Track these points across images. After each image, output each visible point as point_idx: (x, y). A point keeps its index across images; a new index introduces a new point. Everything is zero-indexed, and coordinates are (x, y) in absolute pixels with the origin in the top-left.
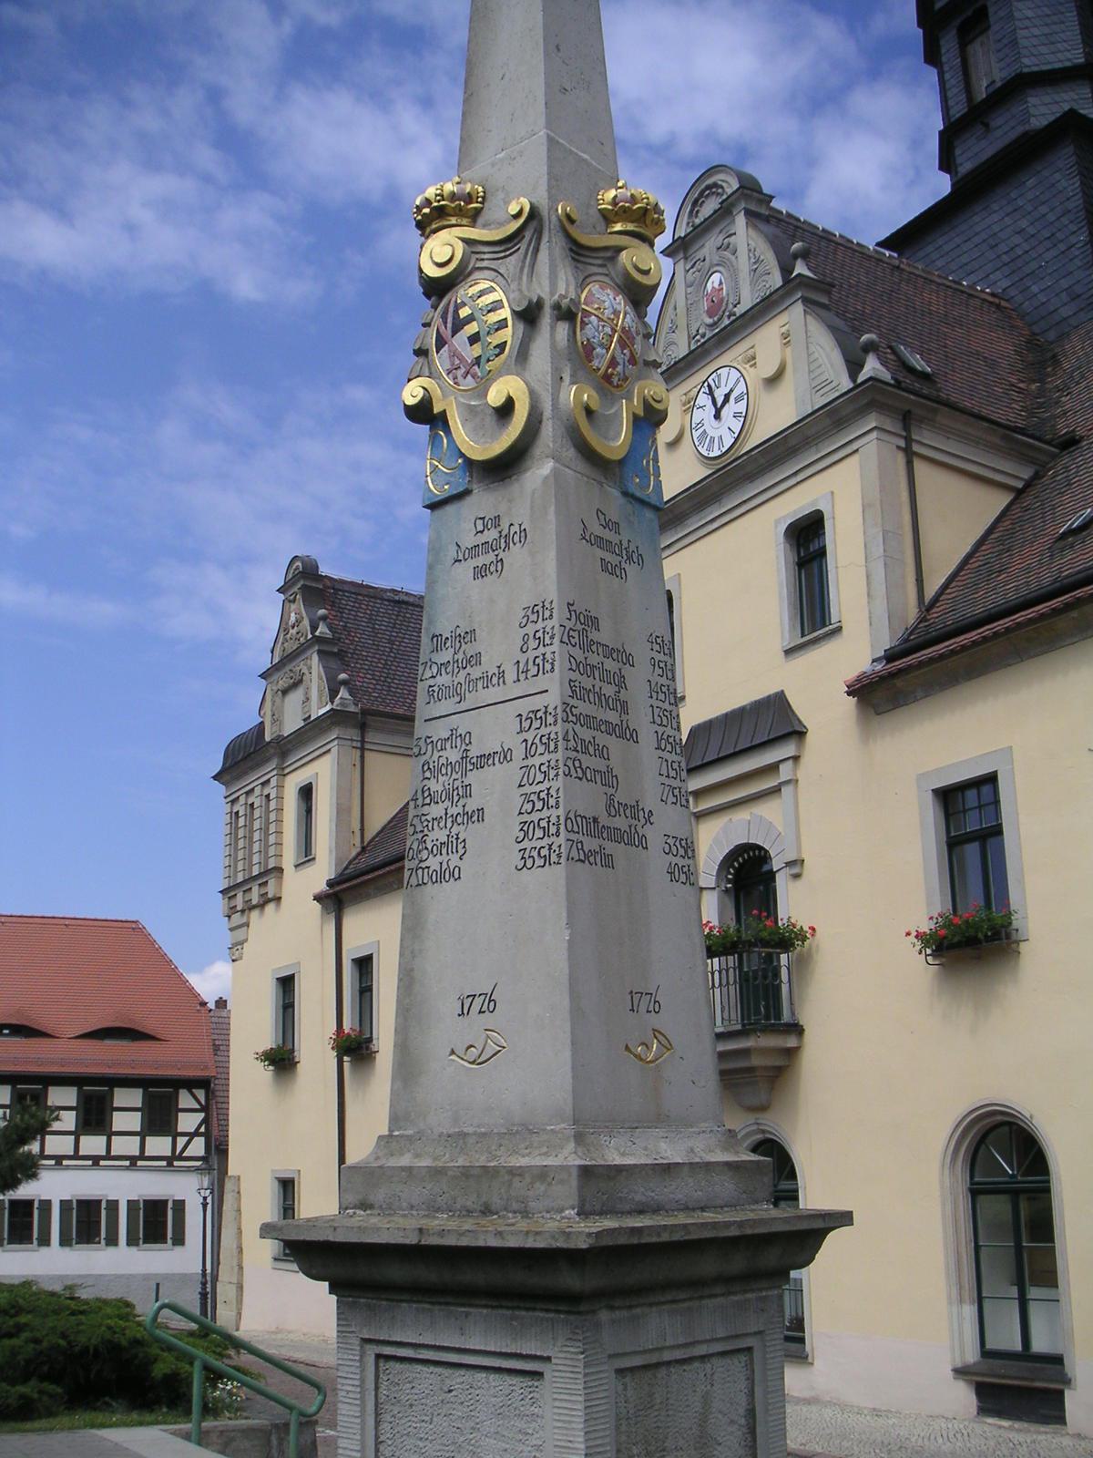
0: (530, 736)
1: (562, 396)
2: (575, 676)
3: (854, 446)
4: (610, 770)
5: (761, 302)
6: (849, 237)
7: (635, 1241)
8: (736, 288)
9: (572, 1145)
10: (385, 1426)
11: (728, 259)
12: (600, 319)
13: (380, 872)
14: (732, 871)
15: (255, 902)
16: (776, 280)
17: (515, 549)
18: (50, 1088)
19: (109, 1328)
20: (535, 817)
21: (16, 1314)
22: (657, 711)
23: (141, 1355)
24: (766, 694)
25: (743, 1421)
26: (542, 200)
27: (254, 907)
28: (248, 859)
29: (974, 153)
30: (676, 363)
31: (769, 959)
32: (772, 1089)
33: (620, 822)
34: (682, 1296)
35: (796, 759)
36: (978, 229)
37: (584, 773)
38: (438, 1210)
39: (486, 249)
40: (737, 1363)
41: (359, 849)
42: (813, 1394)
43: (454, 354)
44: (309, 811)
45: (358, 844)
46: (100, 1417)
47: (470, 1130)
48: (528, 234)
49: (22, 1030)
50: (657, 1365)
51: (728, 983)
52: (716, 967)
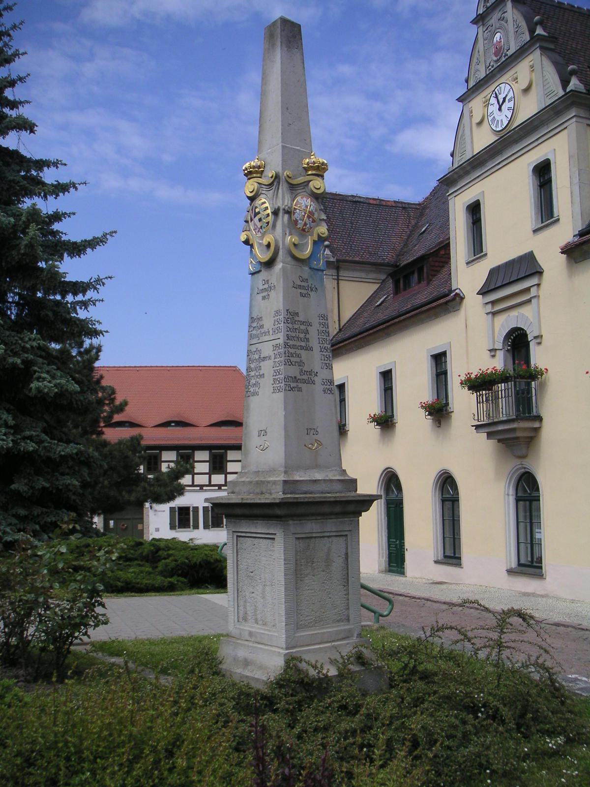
0: (275, 352)
1: (286, 241)
2: (289, 333)
3: (565, 125)
4: (301, 361)
5: (520, 48)
6: (573, 4)
7: (295, 501)
8: (508, 41)
9: (283, 474)
10: (239, 556)
11: (504, 26)
12: (300, 210)
13: (347, 342)
14: (510, 340)
16: (527, 37)
17: (272, 291)
18: (196, 452)
19: (206, 555)
20: (277, 377)
21: (168, 550)
22: (321, 339)
23: (219, 566)
24: (525, 253)
25: (344, 556)
26: (279, 169)
30: (480, 81)
31: (529, 384)
32: (528, 447)
33: (305, 377)
34: (319, 518)
35: (538, 285)
37: (291, 363)
38: (251, 493)
39: (264, 187)
40: (342, 539)
41: (338, 330)
42: (546, 593)
43: (255, 224)
45: (337, 326)
46: (202, 591)
47: (260, 470)
48: (275, 183)
49: (181, 424)
50: (312, 537)
51: (508, 396)
52: (503, 388)
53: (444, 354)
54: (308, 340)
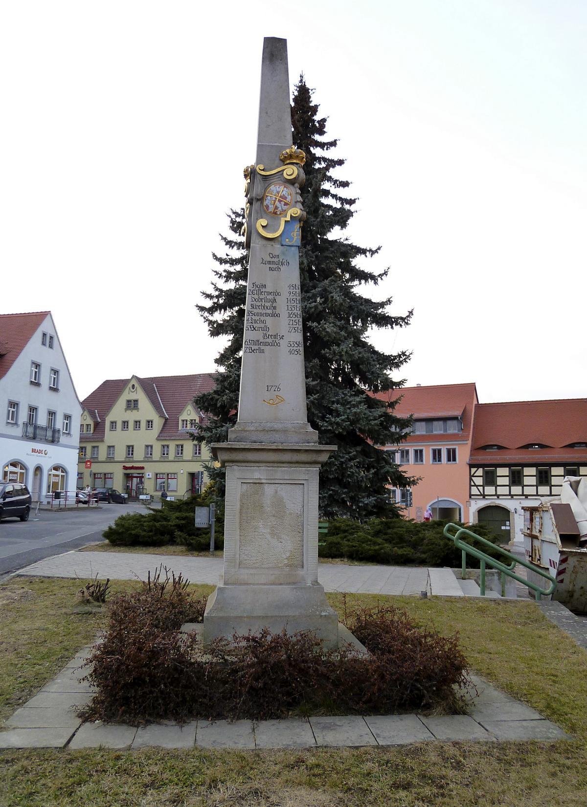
33: (269, 340)
37: (254, 329)
54: (275, 308)
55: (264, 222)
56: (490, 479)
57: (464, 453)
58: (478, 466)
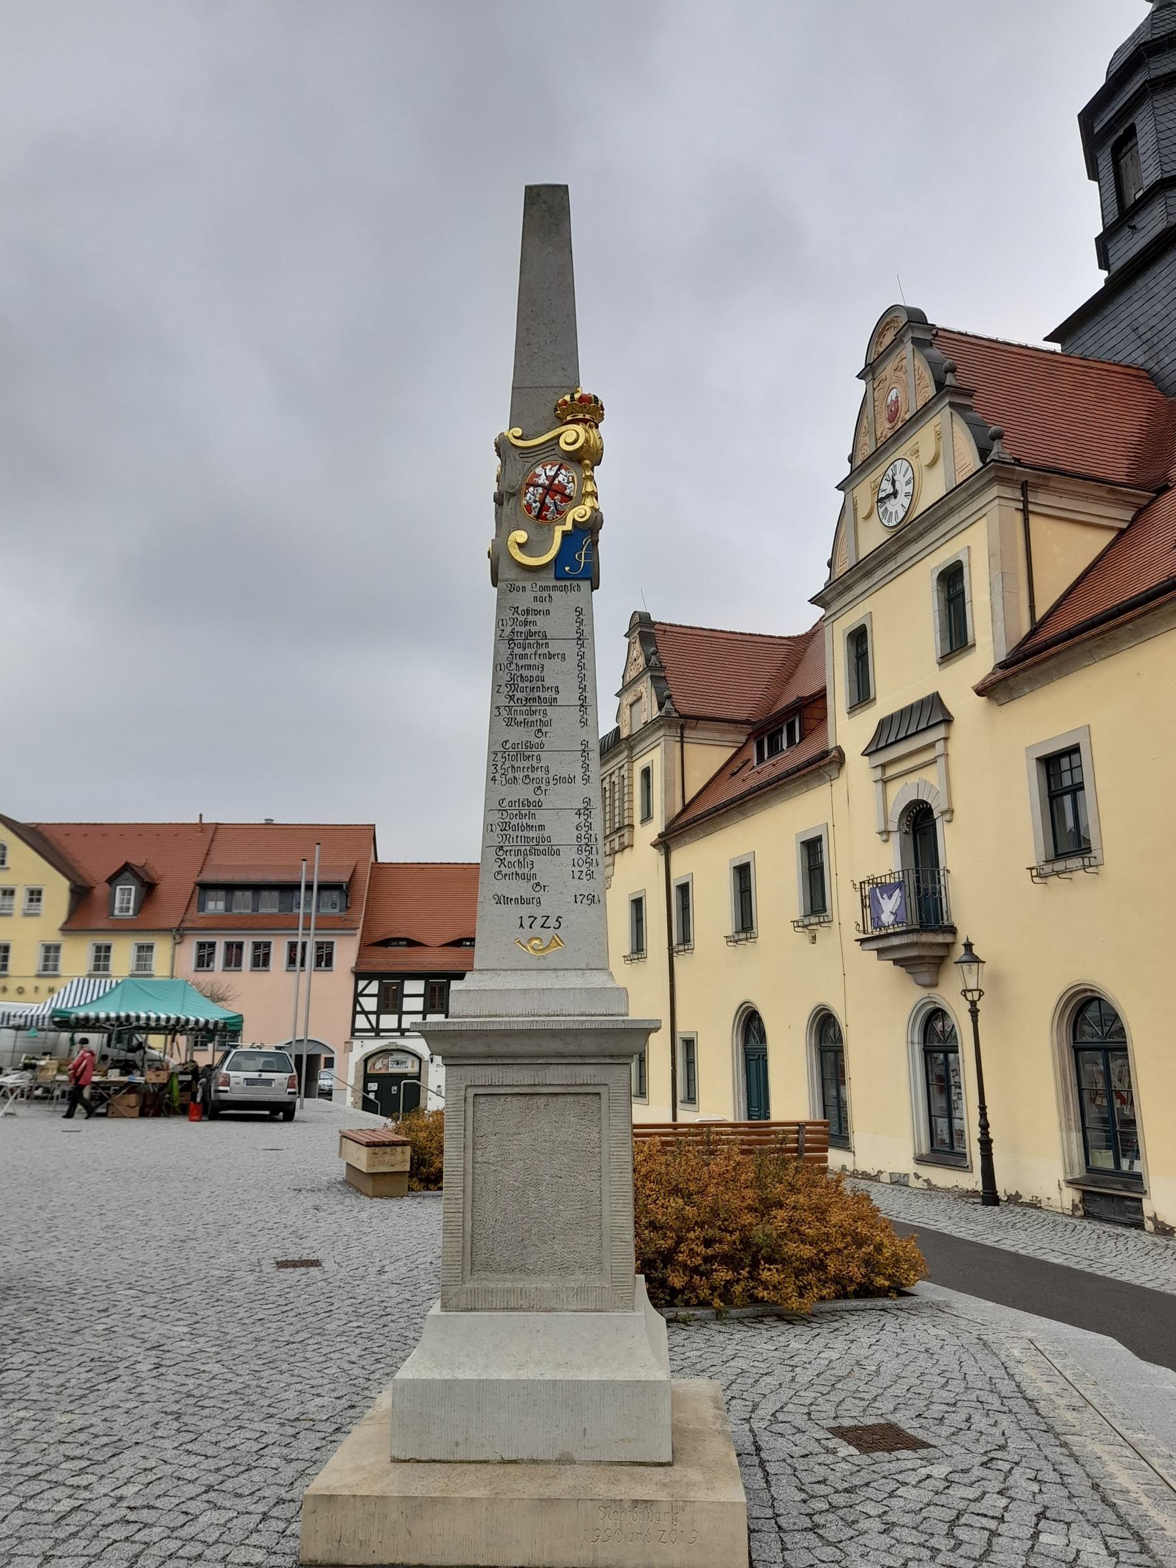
15: (617, 848)
16: (931, 391)
27: (617, 852)
28: (612, 819)
29: (1129, 247)
35: (946, 739)
36: (1122, 317)
44: (648, 787)
53: (819, 839)
55: (521, 536)
56: (390, 1002)
57: (346, 952)
58: (370, 976)
